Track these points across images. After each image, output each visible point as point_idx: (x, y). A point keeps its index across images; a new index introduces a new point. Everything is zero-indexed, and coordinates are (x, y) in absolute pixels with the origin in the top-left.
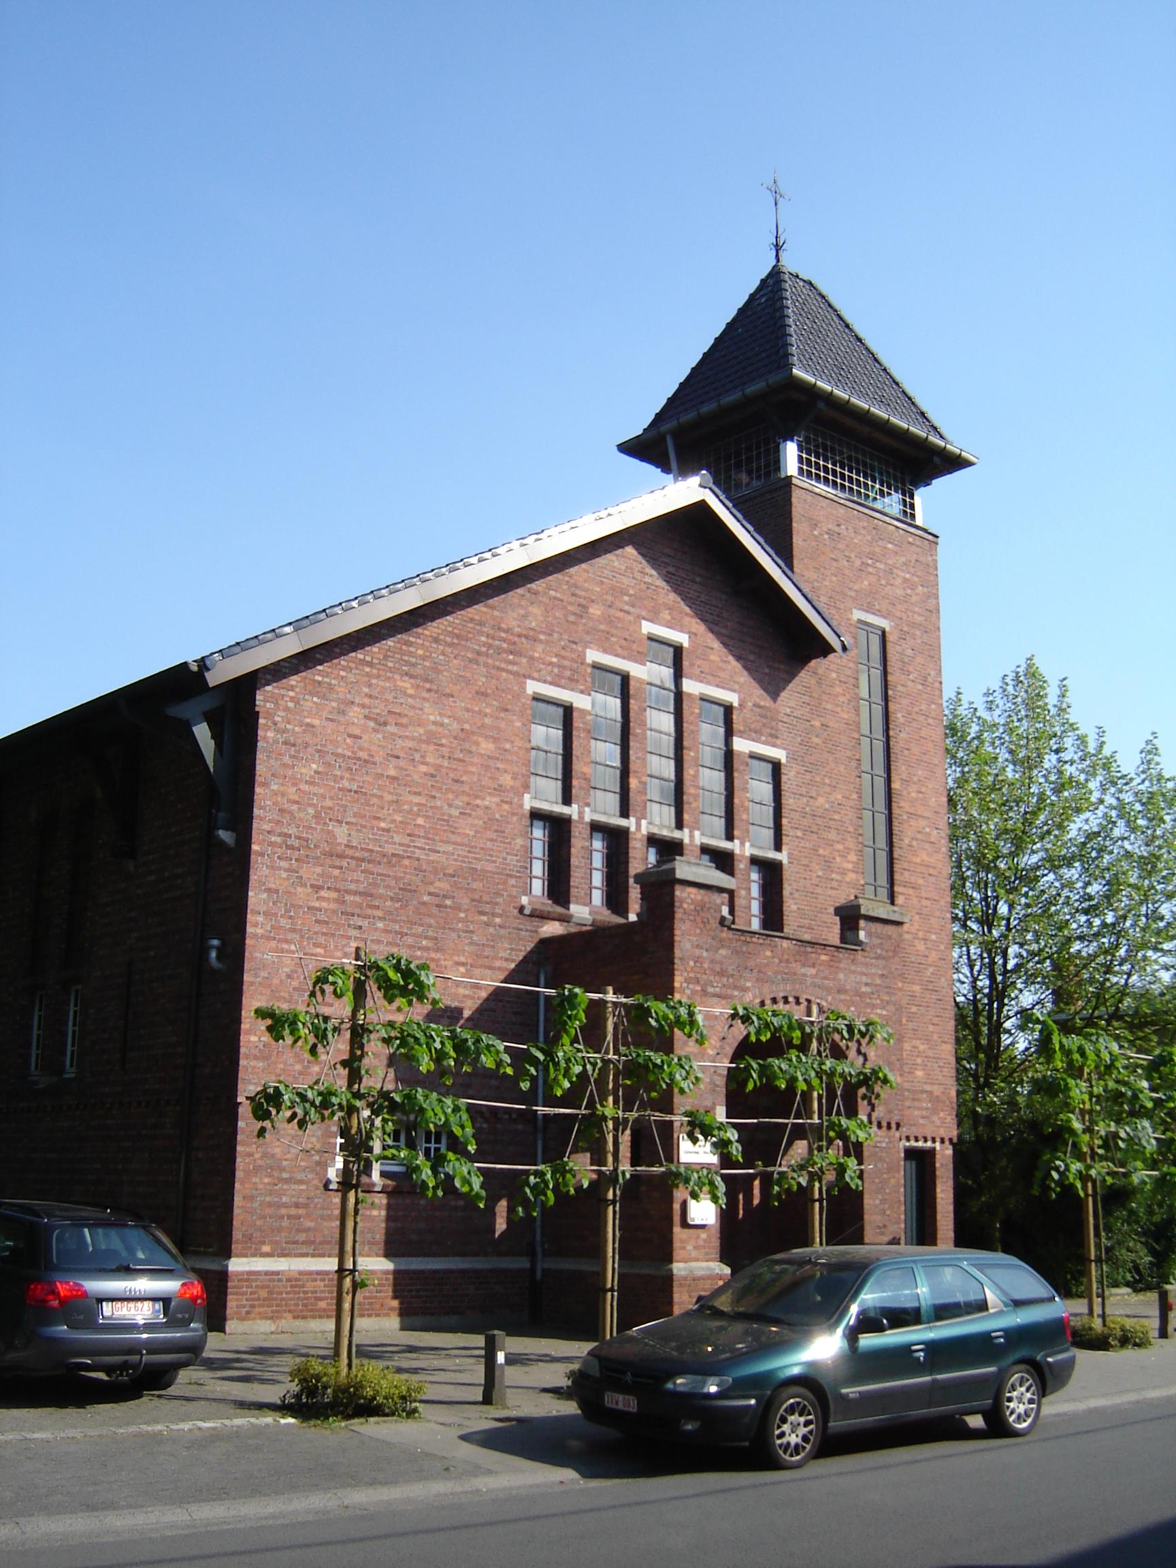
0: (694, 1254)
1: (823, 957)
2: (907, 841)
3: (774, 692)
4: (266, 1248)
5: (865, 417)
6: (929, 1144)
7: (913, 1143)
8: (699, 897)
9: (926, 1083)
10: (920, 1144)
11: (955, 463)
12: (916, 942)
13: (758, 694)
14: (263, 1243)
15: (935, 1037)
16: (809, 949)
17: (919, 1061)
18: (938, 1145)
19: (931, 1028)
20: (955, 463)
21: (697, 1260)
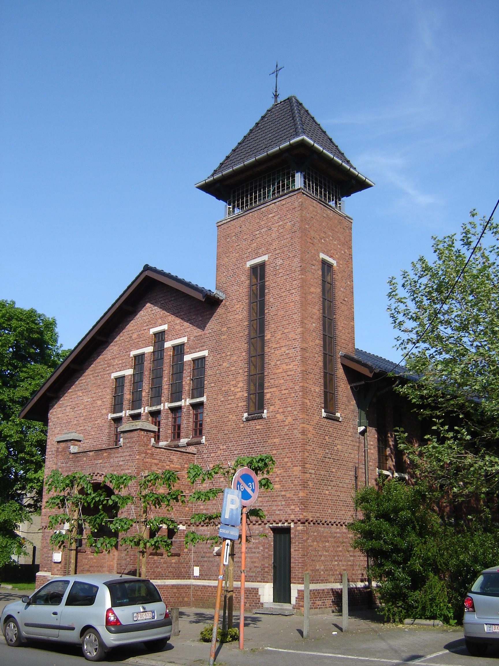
0: (57, 573)
1: (105, 454)
2: (273, 364)
3: (202, 326)
4: (46, 569)
5: (258, 163)
6: (286, 524)
7: (275, 525)
8: (64, 445)
9: (281, 491)
10: (280, 525)
11: (207, 188)
12: (278, 415)
13: (197, 331)
14: (45, 567)
15: (289, 464)
16: (100, 453)
17: (277, 479)
18: (292, 525)
19: (286, 460)
20: (207, 188)
21: (57, 575)
